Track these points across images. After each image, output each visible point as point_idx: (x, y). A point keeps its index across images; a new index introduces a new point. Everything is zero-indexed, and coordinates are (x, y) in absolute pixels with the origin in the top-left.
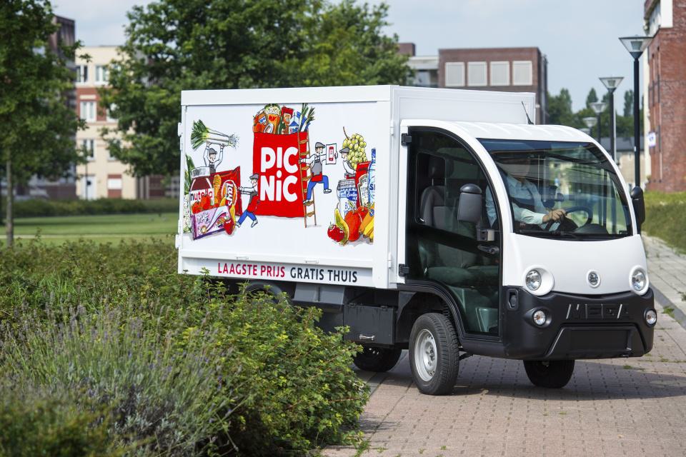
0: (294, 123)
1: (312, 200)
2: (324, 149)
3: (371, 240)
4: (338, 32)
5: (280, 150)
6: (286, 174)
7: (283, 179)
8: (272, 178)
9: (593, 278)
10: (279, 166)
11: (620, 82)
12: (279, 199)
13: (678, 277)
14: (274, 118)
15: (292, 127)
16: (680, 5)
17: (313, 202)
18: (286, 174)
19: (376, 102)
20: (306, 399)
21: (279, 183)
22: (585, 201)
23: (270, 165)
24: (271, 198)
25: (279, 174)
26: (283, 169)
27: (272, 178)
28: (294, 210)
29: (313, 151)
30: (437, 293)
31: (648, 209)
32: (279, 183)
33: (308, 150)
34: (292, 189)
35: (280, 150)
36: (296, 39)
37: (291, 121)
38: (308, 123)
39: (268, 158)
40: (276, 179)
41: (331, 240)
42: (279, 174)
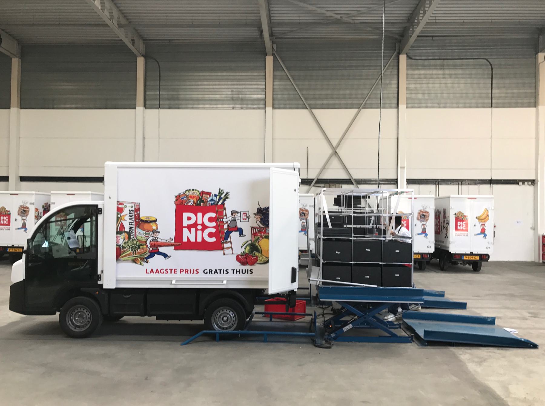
0: (212, 200)
1: (229, 240)
2: (239, 215)
4: (464, 224)
6: (204, 227)
11: (481, 216)
12: (200, 240)
14: (194, 197)
15: (210, 202)
16: (457, 255)
17: (230, 241)
18: (204, 227)
19: (494, 232)
22: (83, 323)
23: (192, 222)
24: (193, 240)
27: (193, 230)
28: (218, 246)
29: (229, 214)
31: (494, 103)
33: (224, 214)
34: (210, 235)
35: (200, 215)
37: (209, 199)
38: (224, 200)
39: (2, 218)
40: (197, 230)
41: (468, 231)
42: (200, 227)
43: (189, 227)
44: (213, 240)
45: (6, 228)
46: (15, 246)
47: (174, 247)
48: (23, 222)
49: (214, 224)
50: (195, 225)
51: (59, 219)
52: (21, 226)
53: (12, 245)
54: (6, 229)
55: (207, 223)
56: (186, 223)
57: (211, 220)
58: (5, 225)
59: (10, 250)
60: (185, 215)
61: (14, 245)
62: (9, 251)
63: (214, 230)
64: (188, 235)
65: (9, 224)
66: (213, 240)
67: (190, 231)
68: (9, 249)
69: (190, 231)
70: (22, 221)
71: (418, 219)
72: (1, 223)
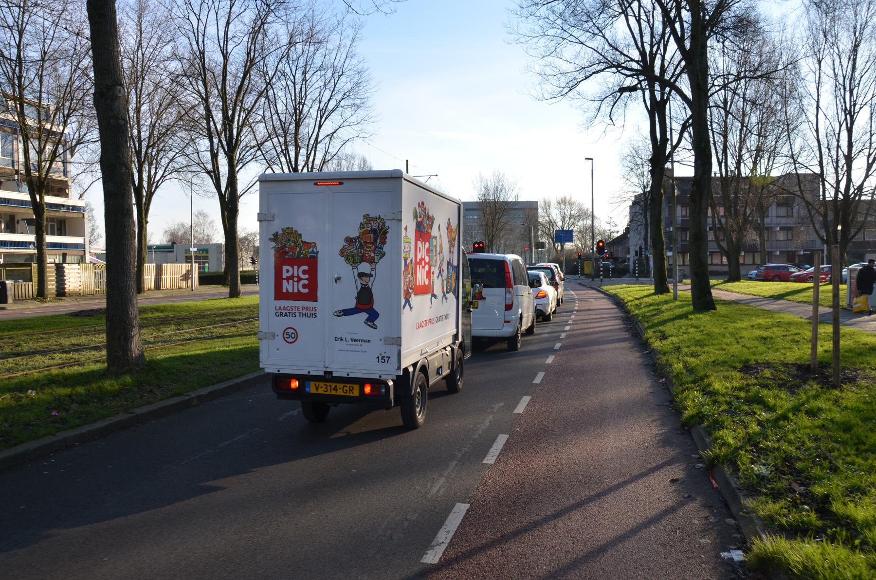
3: (316, 317)
5: (296, 267)
6: (300, 279)
7: (298, 282)
8: (291, 281)
9: (348, 375)
10: (296, 274)
12: (296, 291)
13: (586, 44)
18: (300, 279)
20: (483, 562)
21: (296, 284)
23: (290, 274)
24: (291, 291)
25: (296, 279)
26: (298, 277)
27: (291, 281)
30: (226, 386)
32: (296, 284)
34: (304, 286)
35: (296, 267)
36: (702, 374)
39: (288, 271)
40: (294, 281)
42: (296, 279)
43: (288, 279)
44: (306, 291)
45: (303, 308)
46: (335, 374)
47: (368, 316)
48: (359, 288)
49: (307, 276)
50: (292, 277)
51: (843, 290)
52: (352, 304)
53: (325, 372)
54: (304, 312)
55: (302, 276)
56: (285, 275)
57: (304, 272)
58: (298, 296)
59: (317, 389)
60: (285, 268)
61: (331, 373)
62: (313, 390)
63: (306, 282)
64: (287, 286)
65: (312, 296)
66: (306, 291)
67: (288, 282)
68: (312, 384)
69: (288, 282)
70: (359, 281)
71: (548, 284)
72: (284, 291)
